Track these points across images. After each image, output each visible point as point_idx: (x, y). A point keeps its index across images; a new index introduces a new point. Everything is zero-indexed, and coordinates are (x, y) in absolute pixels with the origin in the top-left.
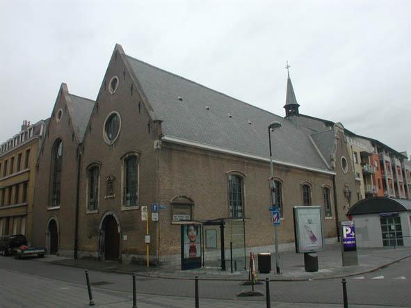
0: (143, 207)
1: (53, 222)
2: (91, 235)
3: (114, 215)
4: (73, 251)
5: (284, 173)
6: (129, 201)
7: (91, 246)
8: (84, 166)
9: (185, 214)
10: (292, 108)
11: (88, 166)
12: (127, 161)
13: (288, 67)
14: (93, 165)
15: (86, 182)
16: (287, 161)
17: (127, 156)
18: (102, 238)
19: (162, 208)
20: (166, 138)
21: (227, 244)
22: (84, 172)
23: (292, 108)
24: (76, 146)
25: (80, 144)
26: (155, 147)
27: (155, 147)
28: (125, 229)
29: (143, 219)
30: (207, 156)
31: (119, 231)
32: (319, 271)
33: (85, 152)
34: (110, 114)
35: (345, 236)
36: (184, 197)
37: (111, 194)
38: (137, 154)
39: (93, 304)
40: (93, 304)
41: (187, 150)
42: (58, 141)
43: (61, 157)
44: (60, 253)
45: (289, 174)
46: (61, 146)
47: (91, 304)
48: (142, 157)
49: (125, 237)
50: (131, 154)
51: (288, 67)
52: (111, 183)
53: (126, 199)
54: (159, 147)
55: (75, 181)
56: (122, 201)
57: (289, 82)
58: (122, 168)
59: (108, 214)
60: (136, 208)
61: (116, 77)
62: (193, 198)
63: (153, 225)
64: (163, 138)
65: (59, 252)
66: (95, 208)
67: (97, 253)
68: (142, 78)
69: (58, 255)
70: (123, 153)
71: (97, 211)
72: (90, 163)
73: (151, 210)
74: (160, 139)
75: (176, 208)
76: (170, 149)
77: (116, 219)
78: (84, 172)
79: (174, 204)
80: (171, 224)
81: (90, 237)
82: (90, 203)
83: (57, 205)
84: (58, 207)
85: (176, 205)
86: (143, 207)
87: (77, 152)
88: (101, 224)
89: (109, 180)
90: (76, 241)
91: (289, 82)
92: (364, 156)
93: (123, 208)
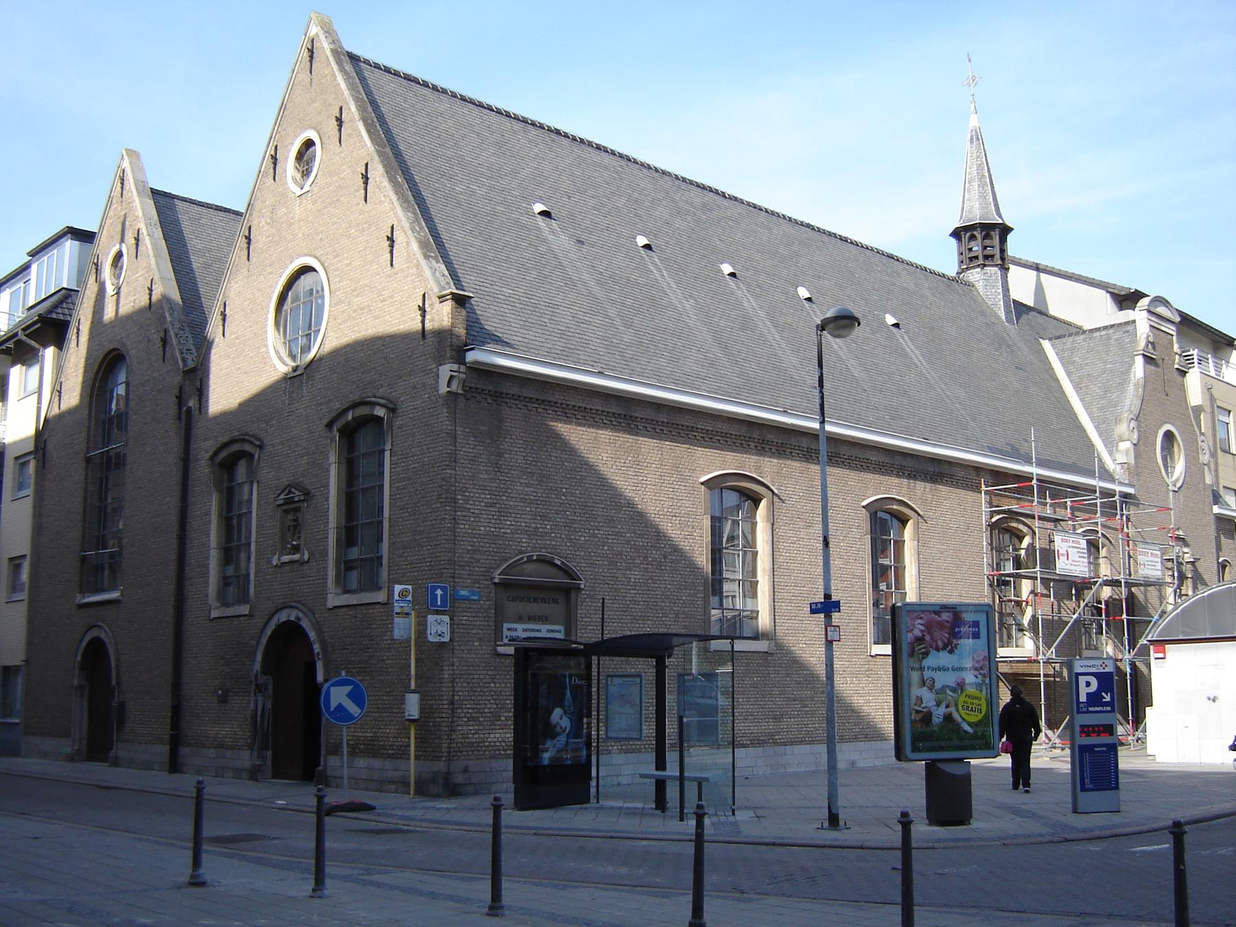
0: (398, 588)
1: (96, 651)
2: (226, 692)
3: (305, 624)
4: (166, 749)
6: (354, 576)
7: (228, 725)
8: (204, 448)
9: (543, 619)
11: (216, 453)
12: (349, 434)
14: (235, 447)
15: (209, 506)
16: (941, 440)
18: (263, 702)
19: (465, 599)
21: (671, 728)
22: (202, 469)
24: (177, 379)
26: (443, 389)
27: (443, 389)
29: (397, 634)
30: (498, 396)
31: (320, 678)
32: (975, 824)
35: (1083, 698)
37: (296, 549)
38: (380, 412)
39: (203, 884)
40: (203, 884)
41: (638, 414)
43: (122, 417)
46: (122, 377)
47: (197, 882)
48: (398, 422)
50: (362, 411)
52: (294, 506)
53: (345, 566)
54: (454, 387)
55: (173, 500)
56: (331, 572)
58: (333, 457)
59: (283, 616)
60: (381, 597)
61: (314, 136)
63: (433, 654)
64: (471, 356)
65: (121, 751)
66: (243, 598)
67: (245, 754)
69: (116, 763)
70: (337, 406)
71: (244, 609)
72: (225, 439)
73: (424, 606)
74: (460, 360)
77: (312, 635)
78: (202, 469)
79: (505, 585)
81: (223, 700)
82: (225, 582)
83: (113, 588)
84: (115, 595)
85: (512, 588)
86: (398, 588)
87: (180, 400)
88: (259, 657)
89: (288, 501)
90: (177, 711)
93: (335, 599)
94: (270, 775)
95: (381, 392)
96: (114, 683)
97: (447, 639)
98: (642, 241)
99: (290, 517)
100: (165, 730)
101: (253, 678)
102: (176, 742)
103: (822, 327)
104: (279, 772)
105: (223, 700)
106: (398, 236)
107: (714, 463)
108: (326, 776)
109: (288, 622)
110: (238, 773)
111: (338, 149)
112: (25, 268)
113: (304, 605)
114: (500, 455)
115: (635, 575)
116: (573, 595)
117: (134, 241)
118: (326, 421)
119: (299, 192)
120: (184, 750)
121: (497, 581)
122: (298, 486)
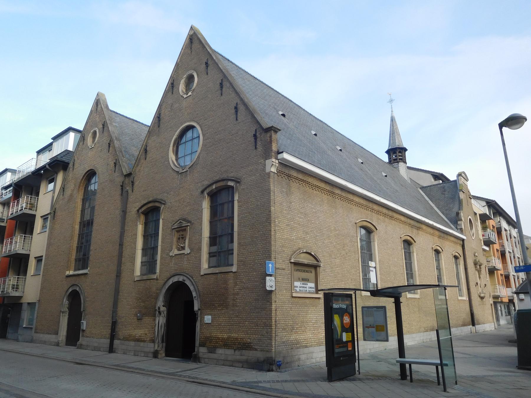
3: (188, 283)
4: (109, 340)
5: (415, 231)
10: (397, 153)
13: (391, 101)
17: (214, 187)
20: (286, 156)
23: (397, 153)
25: (129, 175)
28: (208, 306)
31: (196, 308)
33: (135, 188)
34: (181, 128)
36: (306, 253)
42: (91, 174)
44: (84, 343)
45: (420, 232)
49: (208, 319)
51: (391, 101)
57: (393, 120)
59: (175, 279)
62: (320, 256)
65: (82, 340)
68: (233, 73)
69: (81, 347)
70: (206, 183)
75: (297, 270)
76: (289, 176)
77: (192, 288)
80: (293, 297)
91: (393, 120)
92: (484, 218)
94: (164, 355)
95: (232, 175)
96: (82, 310)
97: (273, 289)
98: (314, 133)
99: (181, 233)
100: (107, 331)
101: (157, 309)
102: (112, 337)
103: (501, 125)
104: (169, 353)
105: (139, 319)
106: (239, 106)
107: (359, 215)
108: (199, 358)
109: (178, 282)
110: (146, 354)
111: (206, 76)
112: (51, 145)
113: (186, 274)
114: (291, 203)
115: (338, 261)
116: (318, 268)
117: (102, 126)
118: (200, 190)
119: (185, 96)
120: (116, 342)
121: (292, 261)
122: (184, 220)
